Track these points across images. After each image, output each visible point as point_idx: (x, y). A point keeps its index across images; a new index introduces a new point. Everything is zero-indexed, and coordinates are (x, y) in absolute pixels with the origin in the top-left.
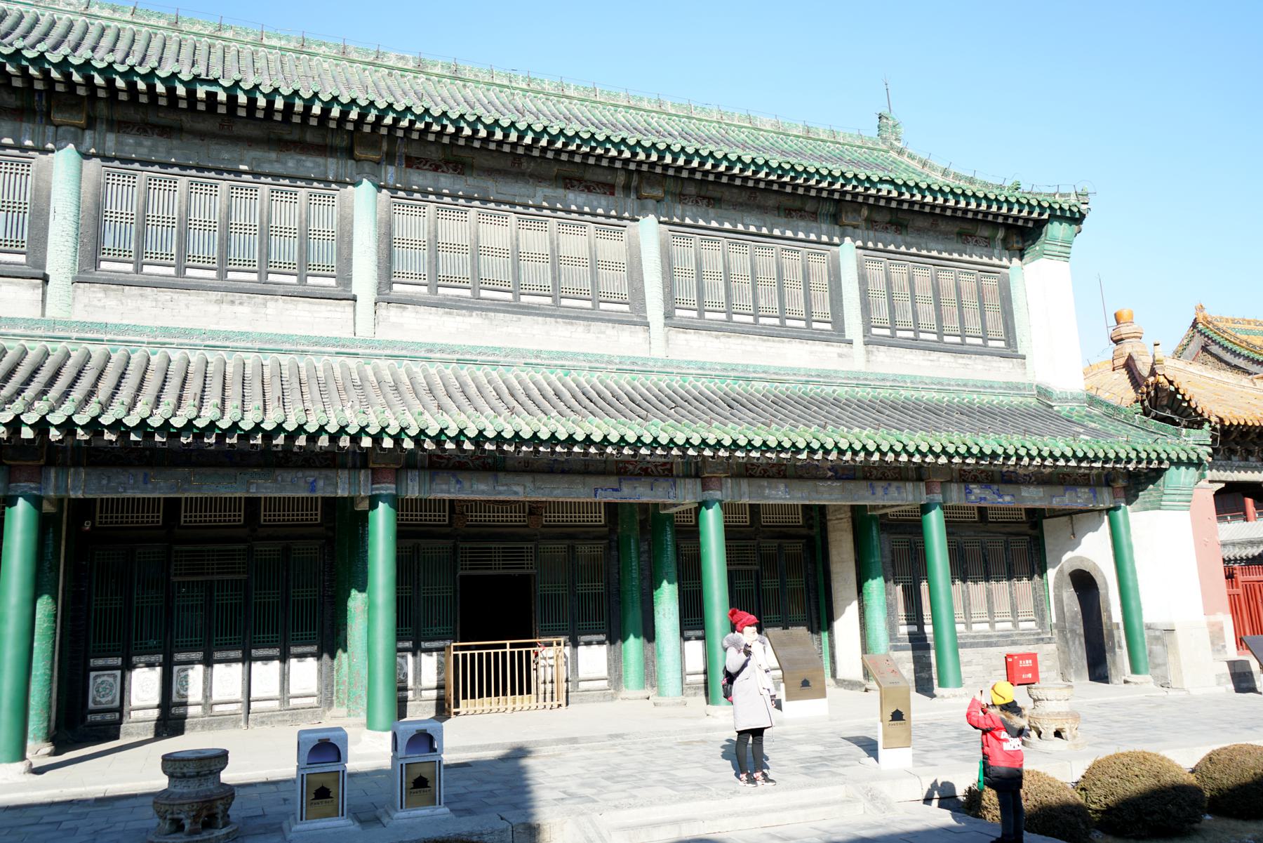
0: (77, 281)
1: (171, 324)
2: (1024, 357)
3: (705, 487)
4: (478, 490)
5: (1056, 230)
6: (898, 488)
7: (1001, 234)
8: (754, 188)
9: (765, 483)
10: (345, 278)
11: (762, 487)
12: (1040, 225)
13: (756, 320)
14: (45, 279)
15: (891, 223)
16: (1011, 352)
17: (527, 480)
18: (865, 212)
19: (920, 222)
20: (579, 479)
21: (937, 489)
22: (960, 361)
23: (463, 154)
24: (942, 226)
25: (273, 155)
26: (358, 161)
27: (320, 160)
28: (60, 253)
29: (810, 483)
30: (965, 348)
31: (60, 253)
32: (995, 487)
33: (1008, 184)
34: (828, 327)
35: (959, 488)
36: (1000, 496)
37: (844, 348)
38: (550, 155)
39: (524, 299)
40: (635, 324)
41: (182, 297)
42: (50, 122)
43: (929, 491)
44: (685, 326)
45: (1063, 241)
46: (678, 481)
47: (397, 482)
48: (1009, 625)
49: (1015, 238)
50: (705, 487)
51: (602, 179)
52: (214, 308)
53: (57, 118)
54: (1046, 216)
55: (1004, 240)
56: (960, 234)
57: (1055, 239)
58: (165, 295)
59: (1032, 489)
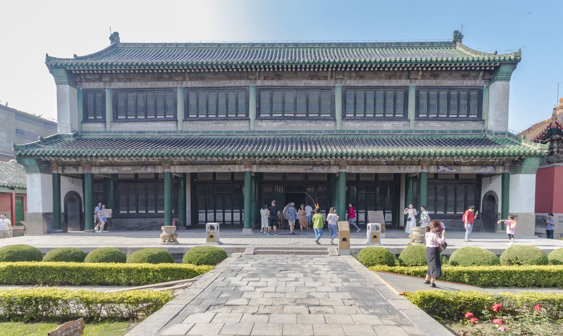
0: (184, 121)
1: (205, 130)
2: (484, 120)
3: (340, 168)
4: (365, 170)
5: (504, 69)
6: (410, 168)
7: (481, 74)
8: (170, 73)
9: (360, 166)
10: (247, 114)
11: (359, 168)
12: (497, 68)
13: (374, 116)
14: (177, 121)
15: (432, 76)
16: (480, 118)
17: (286, 167)
18: (421, 73)
19: (444, 74)
20: (300, 166)
21: (425, 168)
22: (391, 123)
23: (435, 72)
24: (454, 74)
25: (228, 81)
26: (250, 79)
27: (240, 81)
28: (180, 115)
29: (376, 166)
30: (458, 119)
31: (180, 115)
32: (450, 167)
33: (493, 52)
34: (402, 115)
35: (435, 168)
36: (452, 170)
37: (406, 123)
38: (386, 69)
39: (297, 115)
40: (331, 120)
41: (207, 123)
42: (102, 81)
43: (422, 168)
44: (424, 119)
45: (507, 73)
46: (497, 167)
47: (250, 167)
48: (443, 213)
49: (487, 75)
50: (340, 168)
51: (323, 75)
52: (214, 125)
53: (176, 79)
54: (498, 64)
55: (483, 76)
56: (462, 76)
57: (503, 73)
58: (203, 122)
59: (466, 167)
